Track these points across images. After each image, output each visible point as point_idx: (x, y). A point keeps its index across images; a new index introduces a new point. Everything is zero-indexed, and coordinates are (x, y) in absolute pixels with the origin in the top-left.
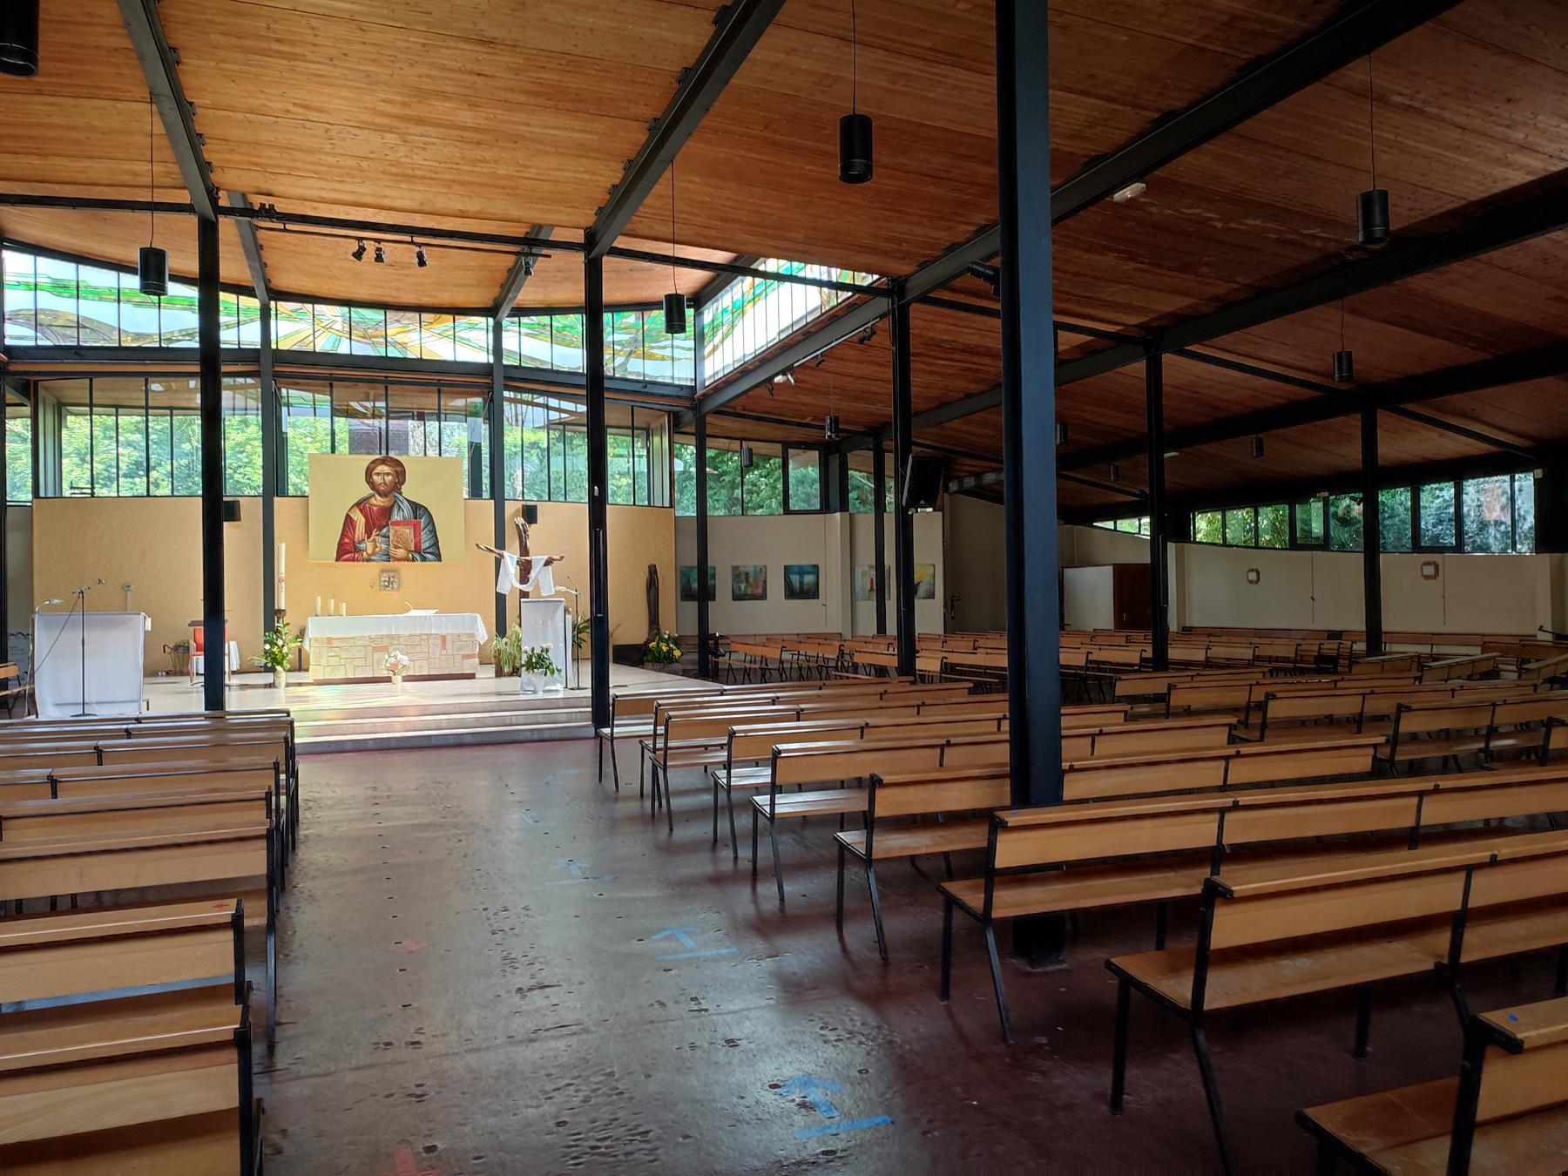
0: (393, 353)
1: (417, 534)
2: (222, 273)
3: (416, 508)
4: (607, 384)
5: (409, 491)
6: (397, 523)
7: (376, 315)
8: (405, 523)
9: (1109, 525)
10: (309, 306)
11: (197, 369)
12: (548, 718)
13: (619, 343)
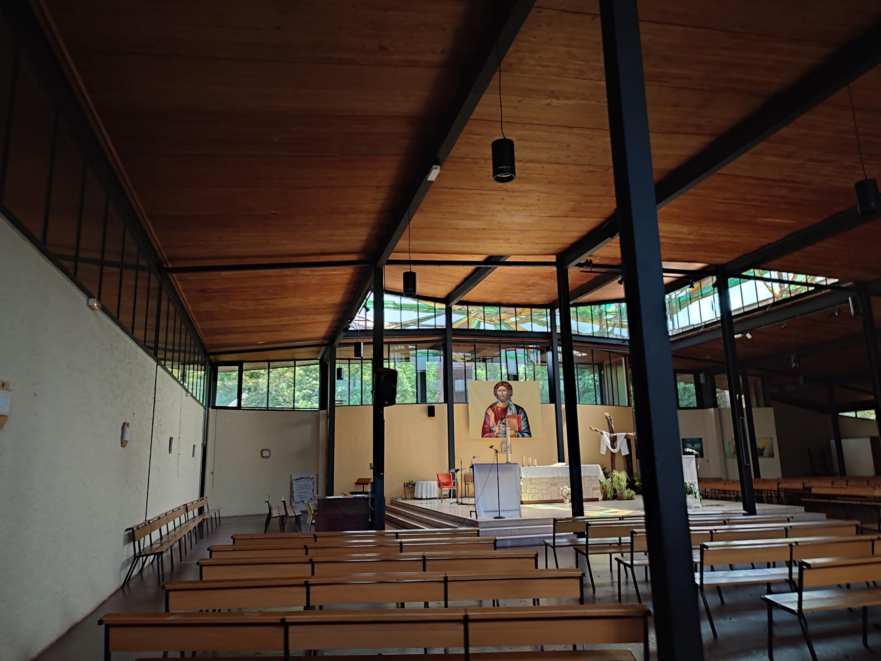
0: (504, 328)
1: (519, 422)
2: (417, 290)
3: (518, 408)
4: (574, 338)
5: (515, 400)
6: (509, 417)
7: (495, 310)
8: (513, 416)
9: (852, 414)
10: (466, 307)
11: (372, 340)
12: (509, 533)
13: (610, 320)
